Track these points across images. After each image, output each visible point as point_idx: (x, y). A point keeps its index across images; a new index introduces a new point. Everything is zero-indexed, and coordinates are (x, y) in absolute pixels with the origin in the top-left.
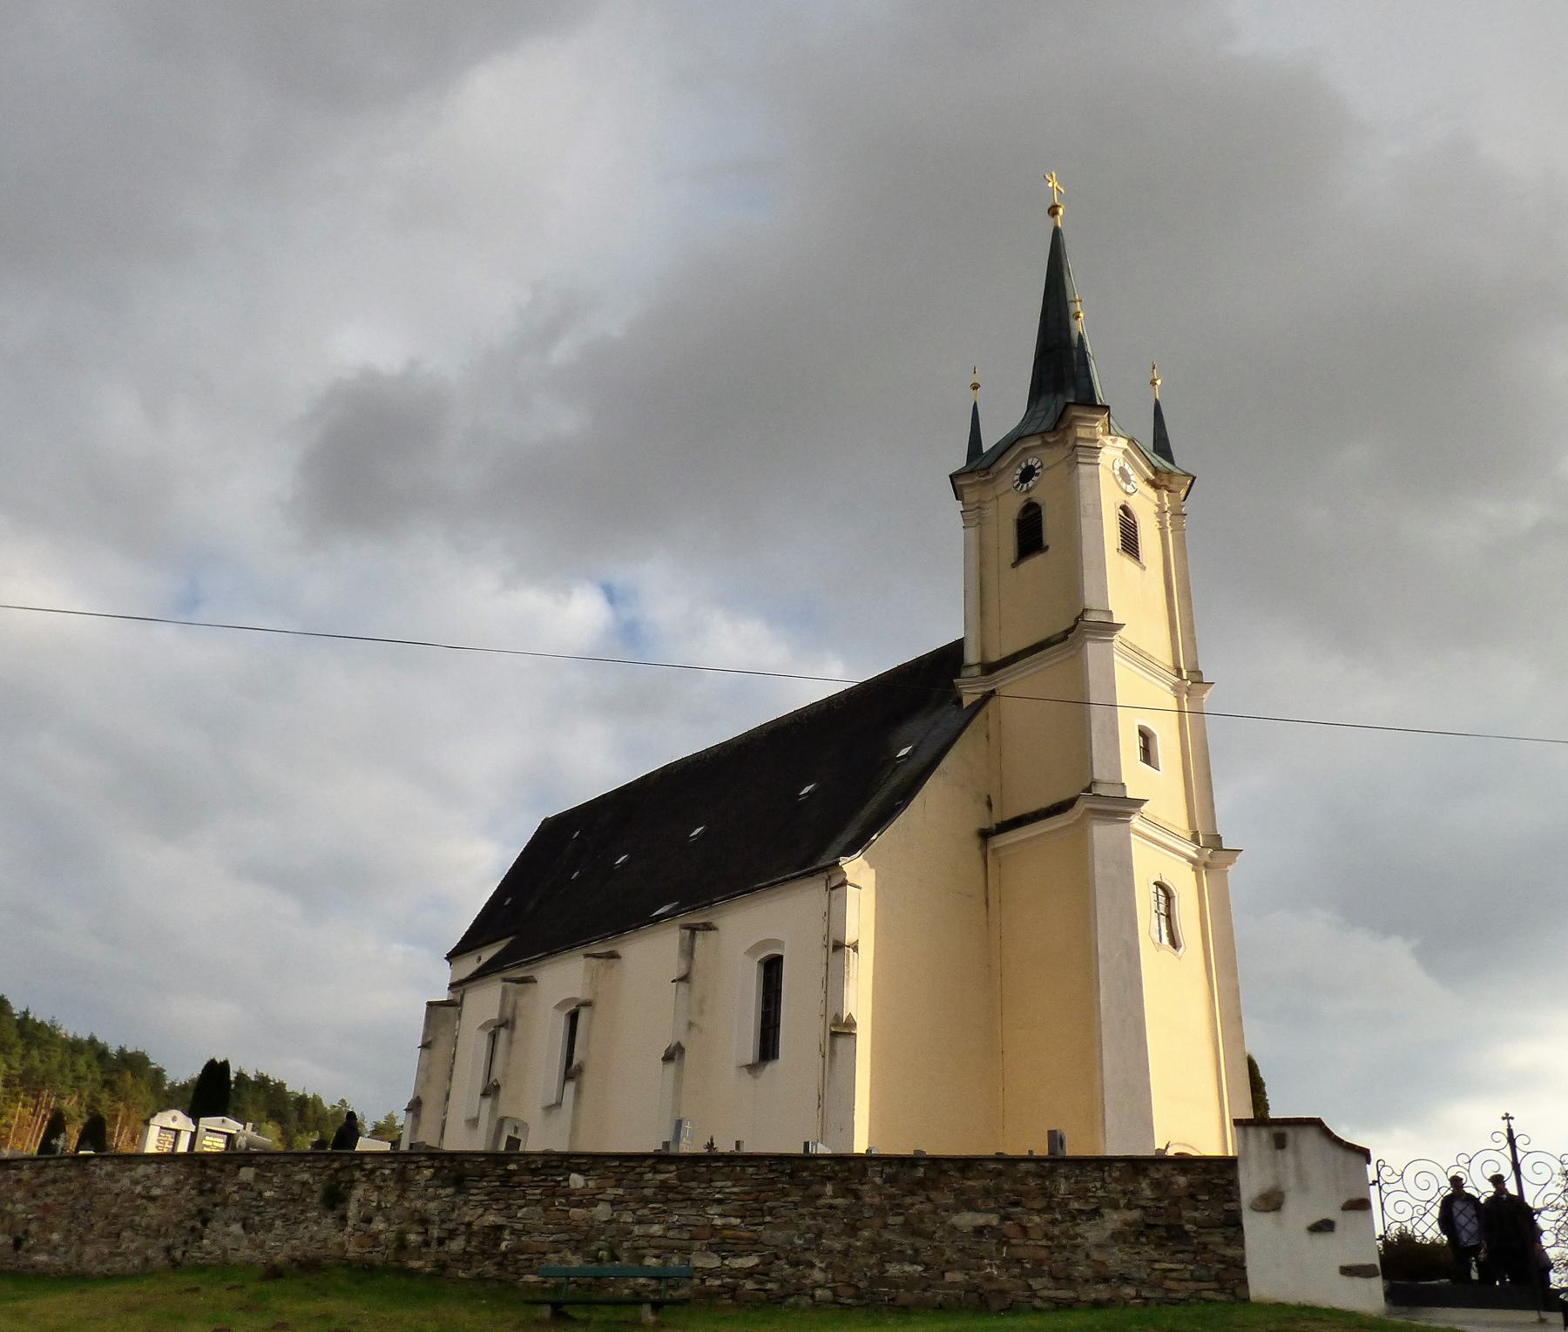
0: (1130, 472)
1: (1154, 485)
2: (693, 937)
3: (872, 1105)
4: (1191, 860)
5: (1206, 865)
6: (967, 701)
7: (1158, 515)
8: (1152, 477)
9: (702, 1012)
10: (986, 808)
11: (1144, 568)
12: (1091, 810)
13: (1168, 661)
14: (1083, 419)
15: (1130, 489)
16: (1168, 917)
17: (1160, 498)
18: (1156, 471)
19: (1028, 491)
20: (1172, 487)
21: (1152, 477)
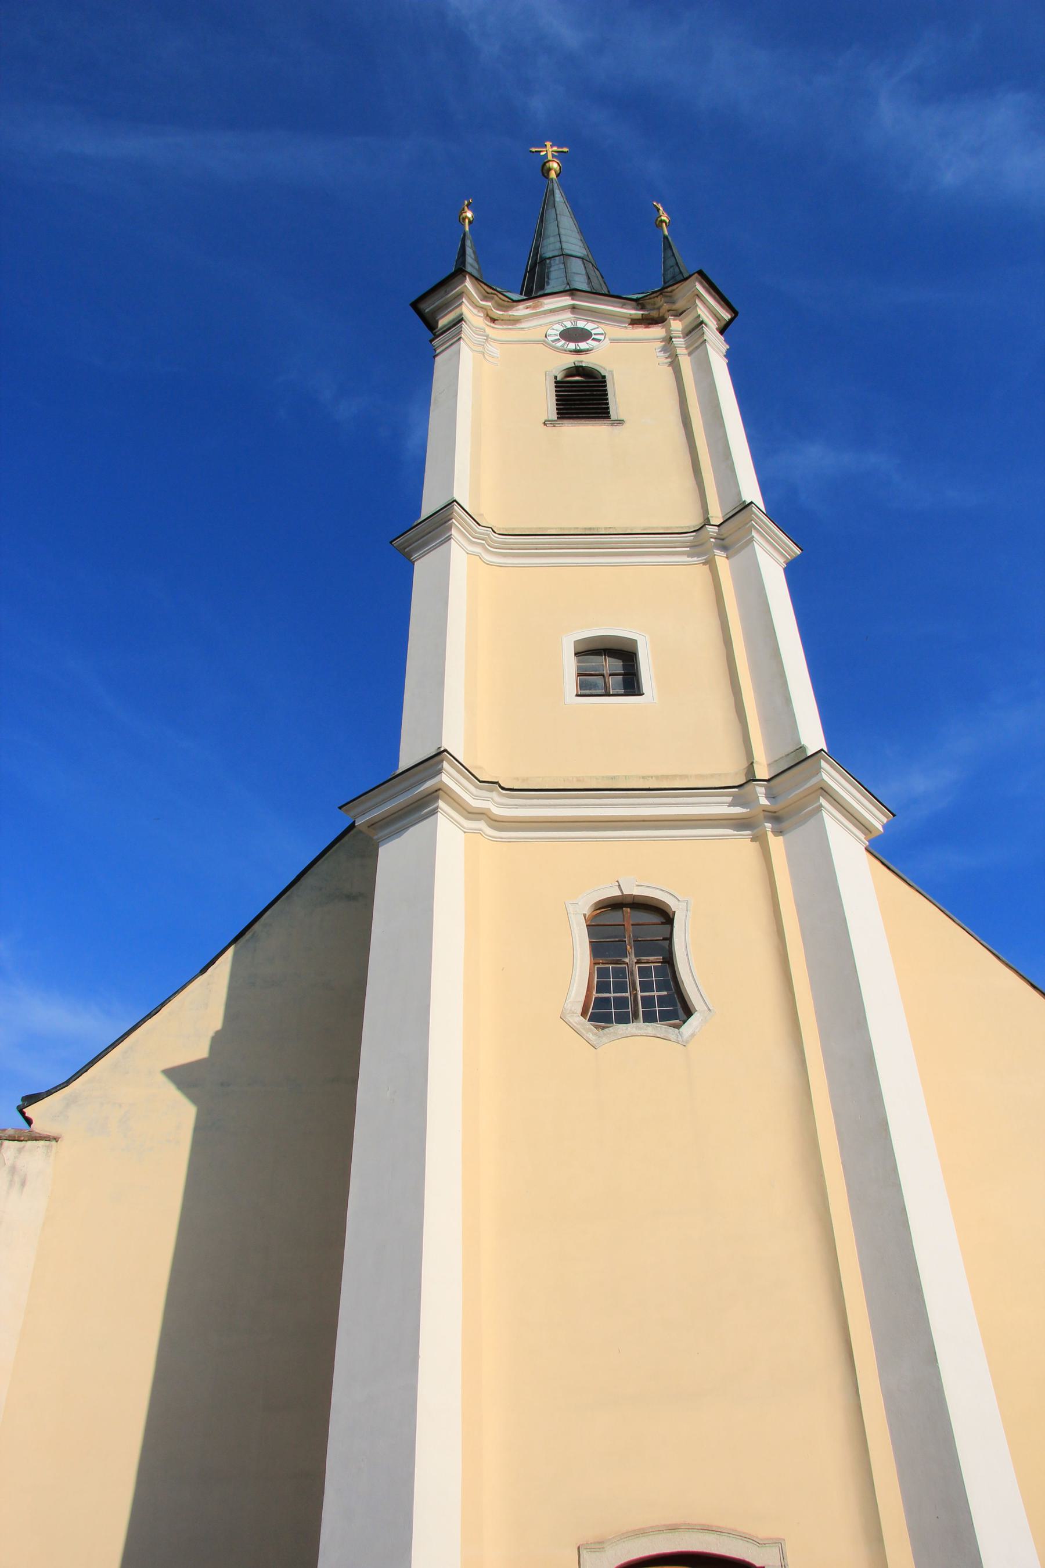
0: (589, 326)
1: (648, 321)
4: (741, 824)
5: (776, 818)
7: (664, 350)
11: (620, 422)
18: (639, 304)
20: (680, 305)
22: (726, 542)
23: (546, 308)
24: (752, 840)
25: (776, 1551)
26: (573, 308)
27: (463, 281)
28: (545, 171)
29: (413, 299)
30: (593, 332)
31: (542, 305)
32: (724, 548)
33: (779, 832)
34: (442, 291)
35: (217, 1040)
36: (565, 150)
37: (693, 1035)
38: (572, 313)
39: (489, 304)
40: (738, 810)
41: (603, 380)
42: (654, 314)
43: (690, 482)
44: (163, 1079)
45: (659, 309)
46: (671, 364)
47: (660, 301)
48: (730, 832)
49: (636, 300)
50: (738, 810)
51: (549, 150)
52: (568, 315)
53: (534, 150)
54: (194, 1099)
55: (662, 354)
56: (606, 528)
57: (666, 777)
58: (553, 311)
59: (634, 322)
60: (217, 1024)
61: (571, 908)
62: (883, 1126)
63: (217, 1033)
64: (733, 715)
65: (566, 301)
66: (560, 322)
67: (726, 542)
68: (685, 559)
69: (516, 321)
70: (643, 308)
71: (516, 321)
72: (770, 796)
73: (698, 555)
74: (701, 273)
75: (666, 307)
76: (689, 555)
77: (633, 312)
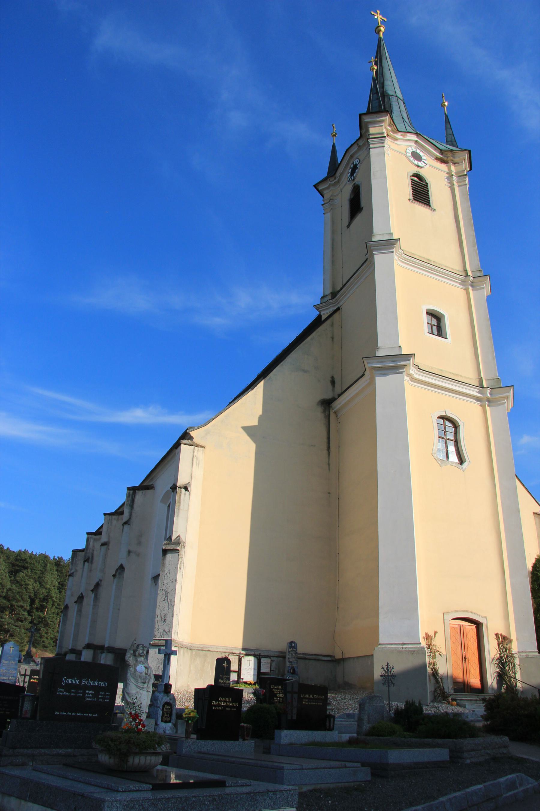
0: (421, 154)
1: (443, 161)
2: (134, 493)
3: (508, 556)
4: (478, 399)
5: (489, 400)
6: (322, 320)
7: (448, 178)
8: (440, 156)
9: (139, 543)
10: (330, 385)
11: (434, 210)
12: (373, 368)
13: (457, 267)
14: (374, 123)
15: (420, 164)
16: (456, 442)
17: (449, 169)
18: (441, 151)
19: (354, 180)
20: (456, 160)
21: (440, 156)
22: (473, 284)
23: (408, 138)
24: (480, 406)
25: (485, 619)
26: (416, 142)
27: (386, 116)
28: (378, 31)
29: (361, 113)
30: (423, 158)
31: (406, 136)
32: (472, 286)
33: (489, 406)
34: (375, 115)
35: (261, 418)
36: (385, 20)
37: (465, 469)
38: (415, 143)
39: (390, 129)
40: (479, 395)
41: (426, 186)
42: (445, 159)
43: (458, 249)
44: (242, 430)
45: (448, 157)
46: (450, 187)
47: (449, 154)
48: (474, 401)
49: (441, 150)
50: (479, 395)
51: (378, 16)
52: (413, 144)
53: (373, 13)
54: (254, 441)
55: (446, 180)
56: (446, 267)
57: (454, 374)
58: (409, 140)
59: (437, 159)
60: (260, 413)
61: (433, 416)
62: (518, 510)
63: (260, 416)
64: (473, 356)
65: (414, 137)
66: (411, 147)
67: (473, 284)
68: (458, 285)
69: (396, 139)
70: (442, 154)
71: (396, 139)
72: (490, 394)
73: (463, 285)
74: (470, 151)
75: (451, 158)
76: (460, 284)
77: (438, 155)
